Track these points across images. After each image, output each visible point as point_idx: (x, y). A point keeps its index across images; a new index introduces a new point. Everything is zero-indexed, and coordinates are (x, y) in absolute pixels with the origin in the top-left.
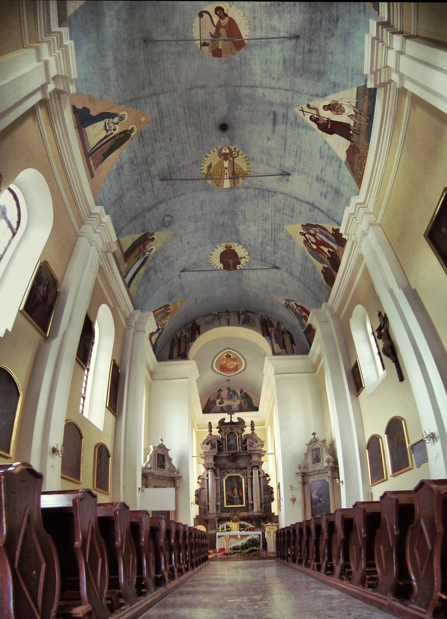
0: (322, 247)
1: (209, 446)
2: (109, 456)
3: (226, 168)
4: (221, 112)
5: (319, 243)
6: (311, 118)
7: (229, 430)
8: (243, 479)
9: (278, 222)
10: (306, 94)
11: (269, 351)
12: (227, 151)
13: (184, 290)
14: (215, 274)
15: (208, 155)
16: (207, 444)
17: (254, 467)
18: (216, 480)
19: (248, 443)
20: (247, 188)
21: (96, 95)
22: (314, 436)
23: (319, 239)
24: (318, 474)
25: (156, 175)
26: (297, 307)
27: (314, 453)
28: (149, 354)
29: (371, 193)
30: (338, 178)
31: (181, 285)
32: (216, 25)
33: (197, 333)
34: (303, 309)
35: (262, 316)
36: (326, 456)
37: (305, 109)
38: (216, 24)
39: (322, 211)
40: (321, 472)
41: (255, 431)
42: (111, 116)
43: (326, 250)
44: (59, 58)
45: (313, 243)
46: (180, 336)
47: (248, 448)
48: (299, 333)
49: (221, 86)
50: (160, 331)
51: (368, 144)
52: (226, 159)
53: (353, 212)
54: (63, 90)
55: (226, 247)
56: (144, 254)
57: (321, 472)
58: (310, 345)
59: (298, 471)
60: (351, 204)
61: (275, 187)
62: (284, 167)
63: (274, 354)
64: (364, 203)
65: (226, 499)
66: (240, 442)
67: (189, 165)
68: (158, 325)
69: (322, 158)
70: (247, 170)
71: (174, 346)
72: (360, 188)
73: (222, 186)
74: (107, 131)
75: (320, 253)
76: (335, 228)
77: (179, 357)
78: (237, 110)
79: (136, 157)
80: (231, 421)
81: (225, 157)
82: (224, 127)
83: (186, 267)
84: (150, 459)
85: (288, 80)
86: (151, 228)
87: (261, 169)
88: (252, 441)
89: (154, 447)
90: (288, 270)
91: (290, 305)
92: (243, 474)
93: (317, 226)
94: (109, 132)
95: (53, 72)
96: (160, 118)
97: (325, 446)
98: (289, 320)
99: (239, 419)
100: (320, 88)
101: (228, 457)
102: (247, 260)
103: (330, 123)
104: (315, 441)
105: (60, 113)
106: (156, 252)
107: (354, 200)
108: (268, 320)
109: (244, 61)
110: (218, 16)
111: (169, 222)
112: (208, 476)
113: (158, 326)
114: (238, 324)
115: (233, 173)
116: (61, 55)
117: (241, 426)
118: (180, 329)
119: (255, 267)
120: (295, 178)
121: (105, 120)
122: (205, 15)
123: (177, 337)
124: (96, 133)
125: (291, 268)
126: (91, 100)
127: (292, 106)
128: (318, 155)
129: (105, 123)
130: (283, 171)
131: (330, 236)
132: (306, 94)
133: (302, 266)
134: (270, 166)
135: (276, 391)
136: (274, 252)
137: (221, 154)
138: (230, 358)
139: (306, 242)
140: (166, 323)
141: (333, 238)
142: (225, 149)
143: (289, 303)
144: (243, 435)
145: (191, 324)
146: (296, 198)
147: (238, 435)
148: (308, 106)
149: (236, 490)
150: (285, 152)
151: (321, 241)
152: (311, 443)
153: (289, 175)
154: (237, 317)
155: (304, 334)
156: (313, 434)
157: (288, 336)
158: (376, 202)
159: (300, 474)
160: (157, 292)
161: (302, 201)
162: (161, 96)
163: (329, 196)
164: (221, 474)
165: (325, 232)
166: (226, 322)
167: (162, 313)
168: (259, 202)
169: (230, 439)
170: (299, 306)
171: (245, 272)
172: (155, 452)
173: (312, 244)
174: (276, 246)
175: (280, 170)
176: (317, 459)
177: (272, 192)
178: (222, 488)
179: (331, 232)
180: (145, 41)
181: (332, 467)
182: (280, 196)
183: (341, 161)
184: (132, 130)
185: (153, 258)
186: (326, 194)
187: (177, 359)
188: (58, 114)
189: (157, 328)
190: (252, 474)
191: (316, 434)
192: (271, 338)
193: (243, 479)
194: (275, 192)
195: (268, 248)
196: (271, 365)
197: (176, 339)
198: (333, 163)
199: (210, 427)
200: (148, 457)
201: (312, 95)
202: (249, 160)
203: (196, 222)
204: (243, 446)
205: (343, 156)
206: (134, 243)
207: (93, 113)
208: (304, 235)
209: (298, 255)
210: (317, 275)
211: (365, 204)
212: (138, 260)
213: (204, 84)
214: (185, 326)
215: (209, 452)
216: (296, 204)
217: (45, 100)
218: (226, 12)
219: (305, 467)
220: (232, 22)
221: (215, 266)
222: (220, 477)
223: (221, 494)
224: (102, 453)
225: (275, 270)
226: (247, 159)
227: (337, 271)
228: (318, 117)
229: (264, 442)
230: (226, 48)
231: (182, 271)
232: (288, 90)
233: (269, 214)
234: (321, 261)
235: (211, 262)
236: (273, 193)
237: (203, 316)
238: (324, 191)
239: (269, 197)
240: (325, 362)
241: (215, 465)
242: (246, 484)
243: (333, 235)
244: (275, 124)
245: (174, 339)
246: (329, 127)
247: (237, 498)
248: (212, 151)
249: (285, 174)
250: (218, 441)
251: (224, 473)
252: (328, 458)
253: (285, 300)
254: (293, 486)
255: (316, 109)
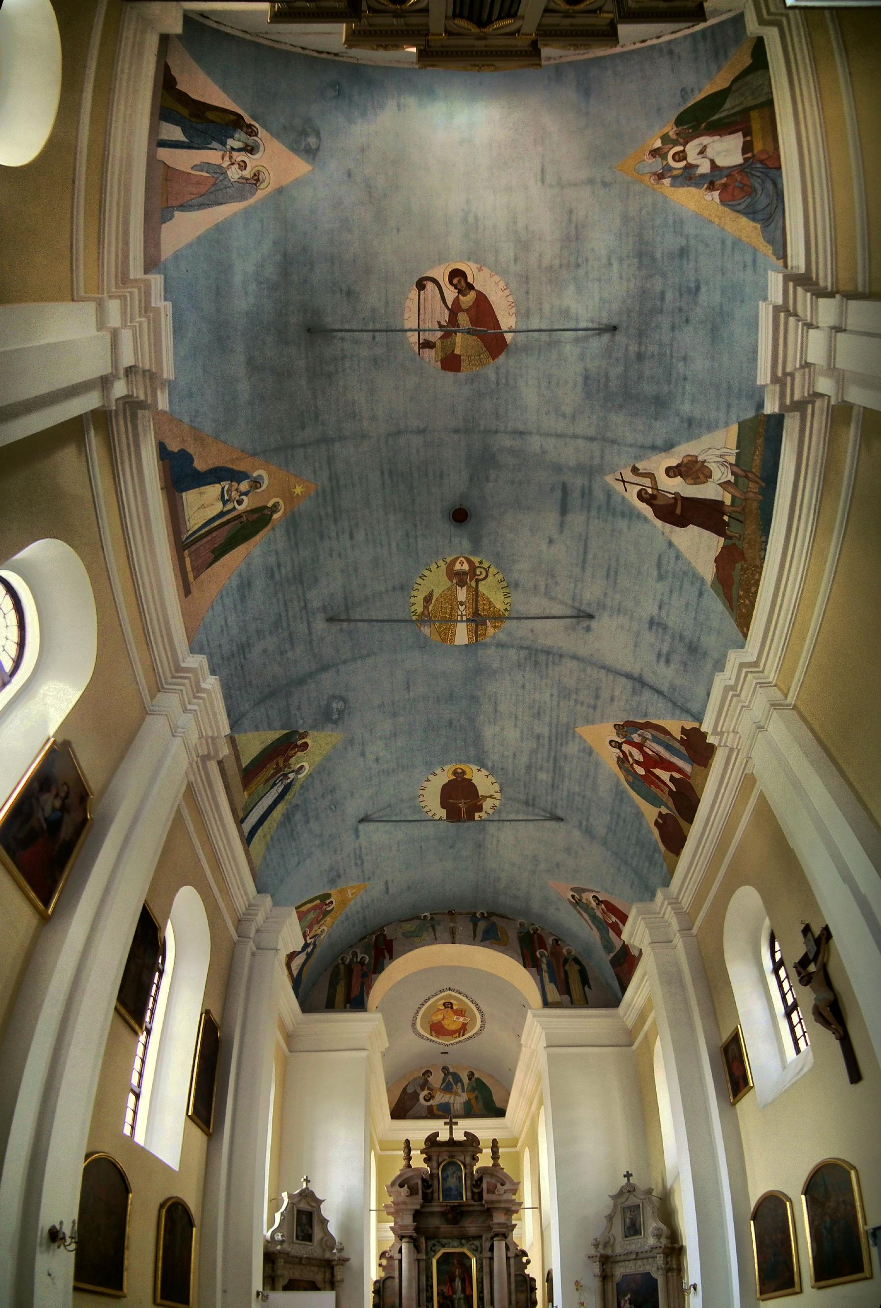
0: (658, 771)
1: (405, 1190)
2: (191, 1225)
3: (462, 604)
4: (455, 485)
5: (651, 762)
6: (640, 496)
7: (446, 1158)
8: (474, 1261)
9: (564, 719)
10: (631, 446)
11: (534, 995)
12: (466, 567)
13: (362, 863)
14: (428, 830)
15: (426, 573)
16: (401, 1186)
17: (496, 1235)
18: (419, 1260)
19: (485, 1186)
20: (501, 645)
21: (208, 427)
22: (628, 1180)
23: (651, 753)
24: (635, 1259)
25: (318, 609)
26: (598, 904)
27: (628, 1215)
28: (285, 999)
29: (779, 615)
30: (695, 619)
31: (358, 853)
32: (450, 305)
33: (387, 956)
34: (611, 908)
35: (521, 925)
36: (651, 1224)
37: (628, 476)
38: (450, 305)
39: (659, 692)
40: (641, 1256)
41: (500, 1161)
42: (236, 476)
43: (665, 776)
44: (141, 330)
45: (637, 762)
46: (352, 960)
47: (486, 1196)
48: (601, 963)
49: (457, 431)
50: (309, 949)
51: (763, 539)
52: (462, 584)
53: (732, 683)
54: (142, 401)
55: (455, 773)
56: (286, 776)
57: (641, 1256)
58: (624, 989)
59: (593, 1252)
60: (729, 666)
61: (560, 645)
62: (581, 600)
63: (546, 1004)
64: (756, 664)
65: (439, 1302)
66: (468, 1182)
67: (387, 591)
68: (305, 936)
69: (661, 577)
70: (504, 607)
71: (338, 979)
72: (745, 636)
73: (452, 641)
74: (225, 503)
75: (652, 783)
76: (688, 727)
77: (348, 1005)
78: (487, 479)
79: (279, 565)
80: (451, 1139)
81: (460, 578)
82: (460, 516)
83: (369, 813)
84: (282, 1221)
85: (595, 417)
86: (301, 722)
87: (536, 605)
88: (493, 1181)
89: (290, 1196)
90: (581, 823)
91: (584, 901)
92: (474, 1250)
93: (648, 726)
94: (229, 507)
95: (127, 359)
96: (332, 489)
97: (651, 1202)
98: (581, 930)
99: (466, 1134)
100: (661, 430)
101: (443, 1214)
102: (497, 803)
103: (679, 503)
104: (629, 1190)
105: (132, 448)
106: (311, 775)
107: (734, 658)
108: (535, 933)
109: (504, 381)
110: (456, 288)
111: (340, 712)
112: (400, 1251)
113: (305, 940)
114: (474, 940)
115: (476, 613)
116: (145, 325)
117: (471, 1149)
118: (351, 946)
119: (512, 817)
120: (604, 624)
121: (223, 484)
122: (429, 285)
123: (343, 963)
124: (203, 505)
125: (588, 819)
126: (198, 436)
127: (601, 470)
128: (655, 573)
129: (223, 488)
130: (579, 610)
131: (677, 745)
132: (631, 446)
133: (612, 813)
134: (552, 599)
135: (547, 1081)
136: (553, 785)
137: (451, 573)
138: (452, 1008)
139: (623, 762)
140: (323, 931)
141: (683, 749)
142: (462, 563)
143: (581, 896)
144: (475, 1168)
145: (374, 937)
146: (603, 667)
147: (465, 1168)
148: (635, 470)
149: (458, 1283)
150: (583, 569)
151: (657, 757)
152: (621, 1193)
153: (591, 617)
154: (471, 927)
155: (610, 966)
156: (625, 1176)
157: (577, 967)
158: (783, 658)
159: (598, 1259)
160: (308, 861)
161: (618, 673)
162: (337, 444)
163: (676, 658)
164: (429, 1249)
165: (665, 738)
166: (447, 935)
167: (315, 911)
168: (527, 675)
169: (448, 1176)
170: (602, 902)
171: (492, 828)
172: (291, 1205)
173: (635, 766)
174: (557, 770)
175: (573, 607)
176: (633, 1229)
177: (554, 656)
178: (429, 1277)
179: (678, 735)
180: (309, 330)
181: (666, 1247)
182: (572, 664)
183: (703, 581)
184: (275, 508)
185: (302, 787)
186: (668, 654)
187: (344, 1009)
188: (130, 454)
189: (303, 942)
190: (491, 1249)
191: (631, 1175)
192: (540, 972)
193: (474, 1261)
194: (561, 656)
195: (543, 776)
196: (539, 1029)
197: (342, 967)
198: (687, 586)
199: (407, 1150)
200: (278, 1216)
201: (642, 447)
202: (510, 586)
203: (394, 715)
204: (475, 1190)
205: (708, 571)
206: (265, 750)
207: (200, 465)
208: (619, 746)
209: (604, 788)
210: (643, 832)
211: (758, 666)
212: (272, 787)
213: (422, 426)
214: (361, 940)
215: (405, 1203)
216: (604, 679)
217: (105, 412)
218: (470, 280)
219: (605, 1245)
220: (482, 300)
221: (430, 814)
222: (427, 1254)
223: (427, 1291)
224: (176, 1220)
225: (553, 824)
226: (504, 584)
227: (690, 820)
228: (655, 492)
229: (518, 1183)
230: (469, 354)
231: (362, 821)
232: (592, 439)
233: (545, 703)
234: (654, 801)
235: (423, 804)
236: (557, 658)
237: (400, 921)
238: (665, 649)
239: (547, 665)
240: (659, 1016)
241: (417, 1229)
242: (480, 1269)
243: (682, 741)
244: (564, 510)
245: (337, 967)
246: (678, 511)
247: (460, 1299)
248: (433, 567)
249: (583, 616)
250: (423, 1180)
251: (434, 1245)
252: (658, 1229)
253: (572, 889)
254: (582, 1282)
255: (651, 476)
